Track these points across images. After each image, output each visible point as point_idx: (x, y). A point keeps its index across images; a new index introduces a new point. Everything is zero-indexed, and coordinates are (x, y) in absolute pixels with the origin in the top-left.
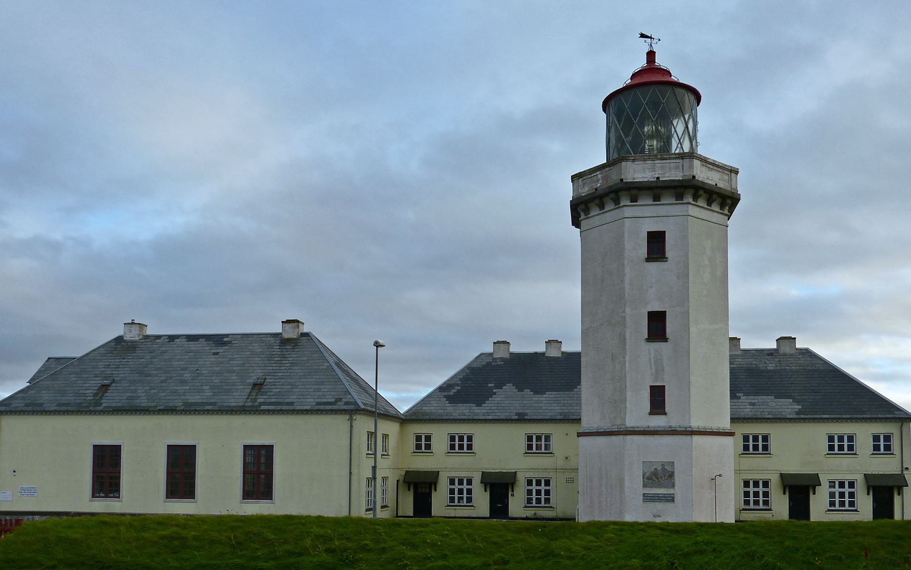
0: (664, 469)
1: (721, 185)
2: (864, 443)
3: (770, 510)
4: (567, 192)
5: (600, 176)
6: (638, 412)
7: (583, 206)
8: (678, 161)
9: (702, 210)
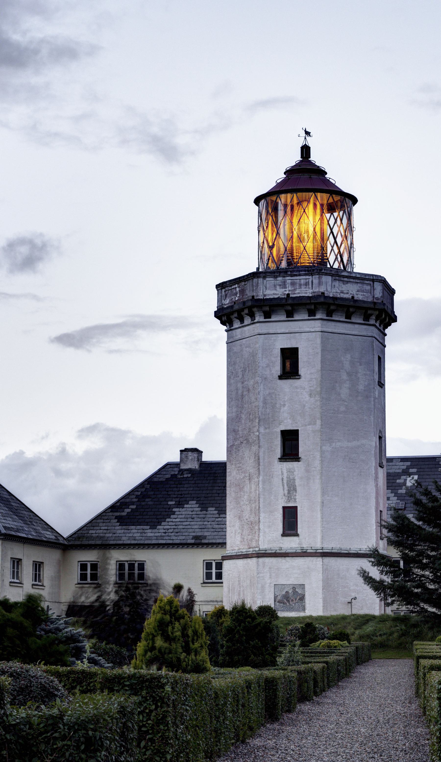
0: (295, 592)
1: (360, 297)
4: (212, 302)
5: (238, 289)
6: (271, 535)
8: (307, 277)
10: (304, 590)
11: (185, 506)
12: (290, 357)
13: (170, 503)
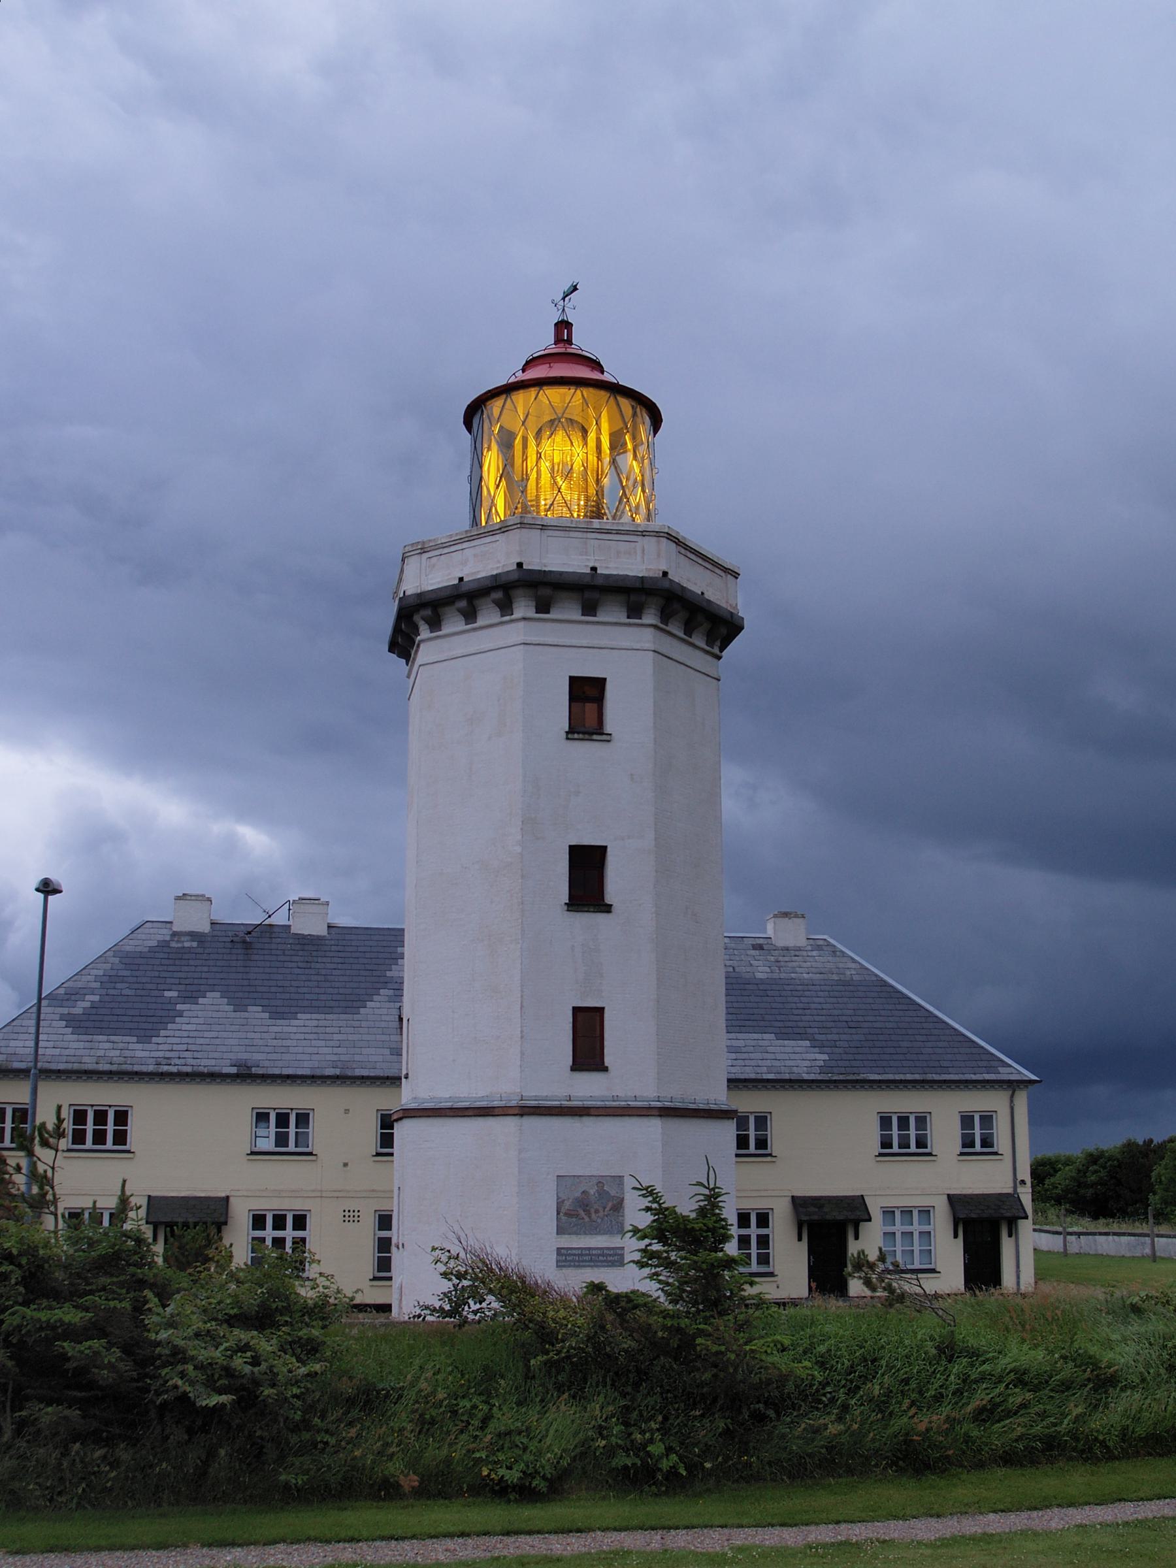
0: (602, 1193)
1: (711, 595)
2: (945, 1134)
3: (772, 1274)
7: (428, 612)
9: (675, 642)
10: (622, 1189)
11: (201, 1000)
12: (587, 695)
13: (167, 994)
